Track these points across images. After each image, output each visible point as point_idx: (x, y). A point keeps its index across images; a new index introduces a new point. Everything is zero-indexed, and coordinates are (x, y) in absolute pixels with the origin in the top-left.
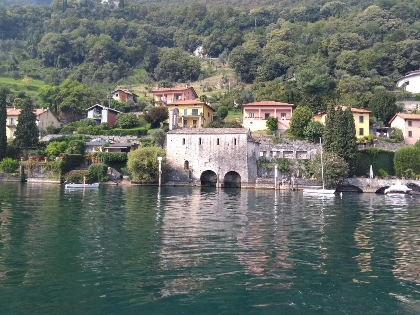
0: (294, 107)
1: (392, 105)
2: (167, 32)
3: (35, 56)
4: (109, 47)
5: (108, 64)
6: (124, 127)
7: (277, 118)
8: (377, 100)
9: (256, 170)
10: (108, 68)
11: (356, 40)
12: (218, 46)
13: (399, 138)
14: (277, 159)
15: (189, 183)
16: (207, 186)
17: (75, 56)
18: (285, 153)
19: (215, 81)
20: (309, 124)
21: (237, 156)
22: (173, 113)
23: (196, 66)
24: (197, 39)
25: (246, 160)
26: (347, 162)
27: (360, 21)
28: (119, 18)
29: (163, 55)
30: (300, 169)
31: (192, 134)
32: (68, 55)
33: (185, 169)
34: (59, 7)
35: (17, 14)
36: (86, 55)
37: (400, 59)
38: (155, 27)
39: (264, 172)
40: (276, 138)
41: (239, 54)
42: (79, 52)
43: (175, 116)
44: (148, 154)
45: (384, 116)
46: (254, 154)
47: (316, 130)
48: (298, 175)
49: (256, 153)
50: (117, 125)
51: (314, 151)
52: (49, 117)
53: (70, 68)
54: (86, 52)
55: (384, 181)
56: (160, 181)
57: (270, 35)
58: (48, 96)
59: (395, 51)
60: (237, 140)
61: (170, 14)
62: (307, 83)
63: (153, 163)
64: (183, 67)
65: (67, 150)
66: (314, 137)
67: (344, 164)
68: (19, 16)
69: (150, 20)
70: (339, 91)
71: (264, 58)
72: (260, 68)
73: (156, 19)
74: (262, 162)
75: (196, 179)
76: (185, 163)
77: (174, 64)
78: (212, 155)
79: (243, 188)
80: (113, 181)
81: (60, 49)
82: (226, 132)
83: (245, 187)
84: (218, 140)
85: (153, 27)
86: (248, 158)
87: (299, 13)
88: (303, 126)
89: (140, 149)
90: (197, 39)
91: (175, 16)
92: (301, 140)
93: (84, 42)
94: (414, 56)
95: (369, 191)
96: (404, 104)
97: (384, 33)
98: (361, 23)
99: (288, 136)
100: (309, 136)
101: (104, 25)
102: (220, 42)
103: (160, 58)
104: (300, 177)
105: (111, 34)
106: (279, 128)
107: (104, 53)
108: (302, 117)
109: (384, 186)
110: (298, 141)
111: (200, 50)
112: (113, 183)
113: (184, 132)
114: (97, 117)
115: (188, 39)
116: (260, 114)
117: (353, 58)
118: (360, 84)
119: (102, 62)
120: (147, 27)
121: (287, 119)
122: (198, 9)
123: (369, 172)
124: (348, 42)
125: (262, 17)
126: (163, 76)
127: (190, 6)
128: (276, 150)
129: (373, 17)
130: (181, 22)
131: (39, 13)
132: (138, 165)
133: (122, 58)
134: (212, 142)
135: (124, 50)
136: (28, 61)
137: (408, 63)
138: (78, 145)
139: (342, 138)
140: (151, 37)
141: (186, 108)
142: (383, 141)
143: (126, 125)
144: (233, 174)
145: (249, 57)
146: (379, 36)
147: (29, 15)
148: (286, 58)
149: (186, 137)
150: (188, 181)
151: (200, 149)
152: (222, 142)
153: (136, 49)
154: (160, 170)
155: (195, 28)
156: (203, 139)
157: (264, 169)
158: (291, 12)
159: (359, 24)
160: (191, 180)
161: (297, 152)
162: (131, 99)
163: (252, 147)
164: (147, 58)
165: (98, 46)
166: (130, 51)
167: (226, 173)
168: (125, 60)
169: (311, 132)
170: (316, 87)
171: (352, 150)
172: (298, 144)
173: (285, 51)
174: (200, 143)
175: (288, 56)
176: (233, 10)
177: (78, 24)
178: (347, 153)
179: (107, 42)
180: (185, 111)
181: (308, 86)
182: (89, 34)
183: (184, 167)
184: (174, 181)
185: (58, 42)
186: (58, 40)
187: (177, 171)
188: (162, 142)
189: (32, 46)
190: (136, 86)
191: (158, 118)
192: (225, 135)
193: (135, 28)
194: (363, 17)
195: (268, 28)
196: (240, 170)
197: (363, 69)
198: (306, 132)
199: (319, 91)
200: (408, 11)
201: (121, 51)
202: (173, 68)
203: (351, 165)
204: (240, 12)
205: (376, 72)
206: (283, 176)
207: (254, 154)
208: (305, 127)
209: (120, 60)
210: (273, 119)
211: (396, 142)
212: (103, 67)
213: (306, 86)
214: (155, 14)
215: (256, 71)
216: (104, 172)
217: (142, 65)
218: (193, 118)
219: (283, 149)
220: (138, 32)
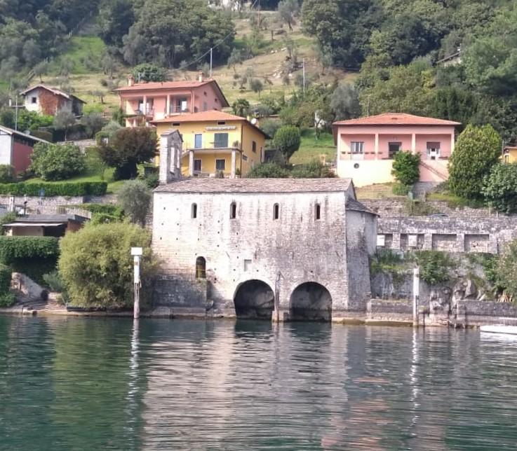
0: (459, 129)
6: (51, 176)
7: (418, 155)
9: (367, 279)
10: (13, 36)
14: (418, 254)
15: (208, 310)
16: (250, 319)
18: (436, 238)
19: (269, 66)
20: (495, 169)
21: (321, 244)
22: (169, 142)
23: (223, 31)
25: (345, 256)
30: (472, 277)
31: (214, 193)
33: (197, 276)
39: (387, 284)
40: (416, 203)
43: (173, 149)
44: (109, 242)
46: (363, 240)
48: (468, 292)
49: (368, 239)
50: (33, 171)
56: (136, 305)
60: (322, 207)
62: (490, 71)
63: (121, 263)
64: (193, 33)
71: (386, 12)
72: (376, 34)
74: (382, 260)
75: (224, 302)
76: (197, 263)
78: (261, 243)
79: (335, 322)
80: (24, 304)
82: (296, 188)
83: (340, 319)
84: (277, 207)
86: (347, 250)
88: (479, 175)
89: (89, 230)
92: (476, 207)
99: (445, 198)
103: (136, 11)
104: (474, 295)
106: (422, 179)
108: (477, 153)
112: (25, 310)
113: (194, 189)
116: (376, 146)
121: (441, 158)
126: (144, 53)
128: (416, 231)
132: (84, 267)
133: (46, 12)
134: (263, 213)
143: (56, 170)
144: (313, 290)
150: (203, 306)
151: (233, 230)
152: (285, 214)
154: (137, 280)
160: (212, 303)
161: (466, 236)
162: (67, 109)
163: (358, 224)
167: (295, 285)
168: (54, 17)
172: (469, 218)
174: (234, 216)
175: (445, 5)
180: (198, 138)
181: (493, 78)
183: (194, 272)
184: (170, 305)
187: (177, 283)
190: (79, 78)
191: (132, 156)
192: (293, 196)
198: (488, 189)
202: (169, 35)
206: (432, 294)
207: (363, 240)
208: (485, 177)
210: (409, 156)
213: (487, 77)
215: (367, 42)
217: (94, 28)
218: (215, 155)
219: (432, 228)
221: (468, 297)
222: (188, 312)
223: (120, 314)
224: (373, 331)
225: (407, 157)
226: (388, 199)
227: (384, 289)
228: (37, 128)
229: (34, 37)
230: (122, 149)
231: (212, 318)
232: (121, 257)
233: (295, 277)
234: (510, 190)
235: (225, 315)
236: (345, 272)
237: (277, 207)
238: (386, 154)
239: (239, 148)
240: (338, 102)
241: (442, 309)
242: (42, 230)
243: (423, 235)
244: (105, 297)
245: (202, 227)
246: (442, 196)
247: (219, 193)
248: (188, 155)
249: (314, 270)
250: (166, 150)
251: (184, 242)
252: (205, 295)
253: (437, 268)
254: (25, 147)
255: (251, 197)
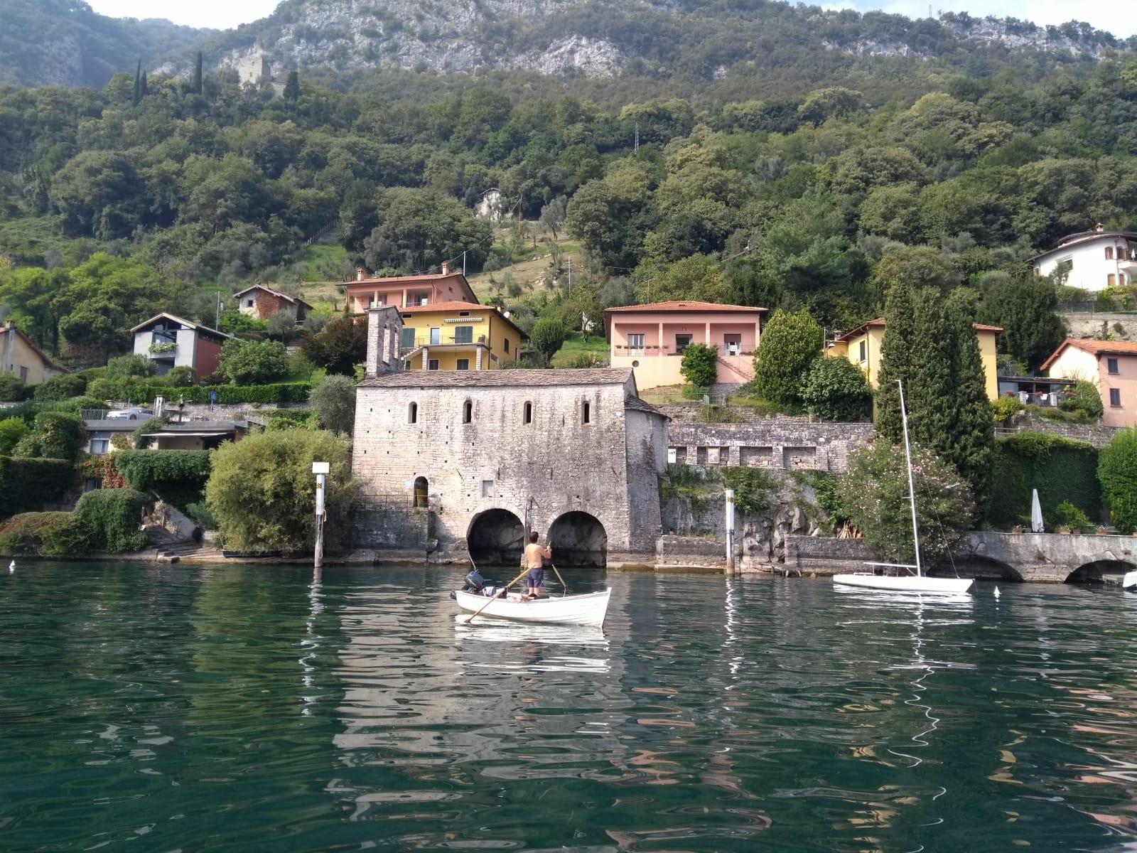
0: (764, 317)
1: (1047, 317)
2: (408, 158)
3: (42, 211)
4: (246, 186)
5: (240, 228)
6: (243, 380)
7: (715, 349)
8: (1002, 301)
9: (656, 506)
10: (239, 239)
11: (905, 164)
12: (539, 190)
13: (1088, 409)
14: (725, 470)
15: (429, 553)
16: (492, 565)
17: (152, 208)
18: (745, 451)
19: (530, 273)
20: (816, 364)
21: (592, 458)
22: (381, 320)
23: (478, 235)
24: (486, 175)
25: (624, 475)
26: (965, 476)
27: (904, 129)
28: (283, 120)
29: (389, 205)
30: (801, 503)
31: (441, 387)
32: (131, 204)
33: (416, 505)
34: (124, 94)
35: (11, 109)
36: (181, 206)
37: (1031, 209)
38: (377, 145)
39: (684, 513)
40: (715, 408)
41: (595, 201)
42: (164, 198)
43: (387, 332)
44: (282, 455)
45: (1026, 347)
46: (649, 451)
47: (840, 382)
48: (796, 524)
49: (656, 451)
50: (221, 376)
51: (839, 448)
52: (10, 350)
53: (136, 241)
54: (184, 200)
55: (1092, 540)
56: (318, 548)
57: (674, 159)
58: (29, 297)
59: (1015, 190)
61: (417, 115)
62: (791, 261)
63: (298, 487)
64: (446, 236)
65: (20, 447)
66: (832, 405)
67: (956, 484)
68: (14, 112)
69: (364, 129)
70: (881, 284)
71: (661, 212)
72: (650, 235)
73: (381, 129)
74: (676, 480)
75: (454, 541)
76: (416, 486)
77: (420, 227)
78: (507, 456)
79: (613, 569)
80: (161, 548)
81: (109, 190)
82: (556, 380)
83: (619, 565)
84: (528, 406)
85: (371, 144)
86: (628, 465)
87: (746, 115)
88: (796, 371)
89: (254, 438)
90: (486, 175)
91: (430, 120)
92: (792, 414)
93: (179, 173)
94: (1068, 201)
95: (1044, 577)
96: (1066, 320)
97: (968, 157)
98: (906, 135)
99: (751, 403)
100: (818, 402)
101: (241, 137)
102: (546, 181)
103: (381, 213)
104: (804, 529)
105: (259, 158)
106: (720, 380)
107: (232, 199)
108: (793, 344)
109: (1094, 559)
110: (781, 418)
111: (493, 201)
112: (161, 557)
113: (413, 383)
114: (163, 351)
115: (461, 175)
116: (660, 338)
117: (906, 204)
118: (940, 263)
119: (224, 223)
120: (355, 144)
121: (742, 353)
122: (488, 104)
123: (1028, 510)
124: (885, 169)
125: (652, 123)
126: (387, 259)
127: (467, 98)
128: (718, 442)
129: (936, 120)
130: (445, 134)
131: (70, 107)
132: (240, 491)
133: (281, 216)
134: (509, 415)
135: (289, 195)
136: (21, 221)
137: (1053, 219)
138: (56, 427)
139: (945, 398)
140: (365, 170)
141: (435, 322)
142: (1043, 415)
143: (249, 373)
144: (579, 524)
145: (622, 209)
146: (955, 165)
147: (44, 110)
148: (722, 209)
149: (417, 396)
150: (423, 548)
151: (467, 439)
153: (322, 194)
154: (319, 510)
155: (481, 150)
156: (478, 404)
157: (684, 502)
158: (725, 114)
159: (902, 136)
160: (436, 543)
161: (785, 449)
162: (290, 313)
163: (642, 428)
164: (346, 213)
165: (215, 181)
166: (306, 200)
167: (555, 516)
168: (290, 222)
169: (822, 387)
170: (815, 272)
171: (978, 438)
172: (786, 428)
173: (719, 192)
174: (468, 419)
175: (727, 204)
176: (577, 106)
177: (170, 133)
178: (964, 448)
179: (241, 174)
181: (795, 268)
182: (193, 156)
183: (412, 498)
184: (373, 547)
185: (106, 172)
186: (104, 166)
187: (386, 514)
188: (343, 419)
189: (37, 182)
190: (313, 286)
191: (344, 351)
192: (551, 390)
193: (325, 148)
194: (911, 119)
195: (668, 148)
196: (603, 507)
197: (935, 235)
198: (808, 390)
199: (823, 284)
200: (1024, 106)
201: (278, 198)
202: (417, 238)
203: (977, 491)
204: (597, 111)
205: (972, 241)
206: (746, 528)
207: (649, 451)
208: (804, 374)
209: (274, 220)
210: (703, 350)
211: (1082, 420)
212: (223, 237)
213: (788, 268)
214: (377, 114)
215: (641, 244)
216: (127, 517)
217: (334, 236)
218: (456, 354)
219: (739, 439)
220: (329, 155)
221: (797, 531)
222: (400, 556)
223: (301, 561)
224: (355, 278)
225: (701, 351)
226: (678, 404)
227: (679, 521)
228: (244, 330)
229: (263, 240)
230: (333, 344)
231: (436, 565)
232: (299, 477)
233: (555, 505)
234: (838, 390)
235: (455, 560)
236: (625, 497)
237: (528, 406)
238: (673, 349)
239: (486, 344)
240: (610, 298)
241: (761, 549)
242: (202, 443)
243: (727, 448)
244: (272, 536)
245: (424, 436)
246: (746, 400)
247: (448, 387)
248: (421, 354)
249: (582, 495)
250: (376, 330)
251: (397, 456)
252: (426, 531)
253: (750, 492)
254: (212, 344)
255: (493, 392)
